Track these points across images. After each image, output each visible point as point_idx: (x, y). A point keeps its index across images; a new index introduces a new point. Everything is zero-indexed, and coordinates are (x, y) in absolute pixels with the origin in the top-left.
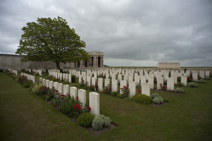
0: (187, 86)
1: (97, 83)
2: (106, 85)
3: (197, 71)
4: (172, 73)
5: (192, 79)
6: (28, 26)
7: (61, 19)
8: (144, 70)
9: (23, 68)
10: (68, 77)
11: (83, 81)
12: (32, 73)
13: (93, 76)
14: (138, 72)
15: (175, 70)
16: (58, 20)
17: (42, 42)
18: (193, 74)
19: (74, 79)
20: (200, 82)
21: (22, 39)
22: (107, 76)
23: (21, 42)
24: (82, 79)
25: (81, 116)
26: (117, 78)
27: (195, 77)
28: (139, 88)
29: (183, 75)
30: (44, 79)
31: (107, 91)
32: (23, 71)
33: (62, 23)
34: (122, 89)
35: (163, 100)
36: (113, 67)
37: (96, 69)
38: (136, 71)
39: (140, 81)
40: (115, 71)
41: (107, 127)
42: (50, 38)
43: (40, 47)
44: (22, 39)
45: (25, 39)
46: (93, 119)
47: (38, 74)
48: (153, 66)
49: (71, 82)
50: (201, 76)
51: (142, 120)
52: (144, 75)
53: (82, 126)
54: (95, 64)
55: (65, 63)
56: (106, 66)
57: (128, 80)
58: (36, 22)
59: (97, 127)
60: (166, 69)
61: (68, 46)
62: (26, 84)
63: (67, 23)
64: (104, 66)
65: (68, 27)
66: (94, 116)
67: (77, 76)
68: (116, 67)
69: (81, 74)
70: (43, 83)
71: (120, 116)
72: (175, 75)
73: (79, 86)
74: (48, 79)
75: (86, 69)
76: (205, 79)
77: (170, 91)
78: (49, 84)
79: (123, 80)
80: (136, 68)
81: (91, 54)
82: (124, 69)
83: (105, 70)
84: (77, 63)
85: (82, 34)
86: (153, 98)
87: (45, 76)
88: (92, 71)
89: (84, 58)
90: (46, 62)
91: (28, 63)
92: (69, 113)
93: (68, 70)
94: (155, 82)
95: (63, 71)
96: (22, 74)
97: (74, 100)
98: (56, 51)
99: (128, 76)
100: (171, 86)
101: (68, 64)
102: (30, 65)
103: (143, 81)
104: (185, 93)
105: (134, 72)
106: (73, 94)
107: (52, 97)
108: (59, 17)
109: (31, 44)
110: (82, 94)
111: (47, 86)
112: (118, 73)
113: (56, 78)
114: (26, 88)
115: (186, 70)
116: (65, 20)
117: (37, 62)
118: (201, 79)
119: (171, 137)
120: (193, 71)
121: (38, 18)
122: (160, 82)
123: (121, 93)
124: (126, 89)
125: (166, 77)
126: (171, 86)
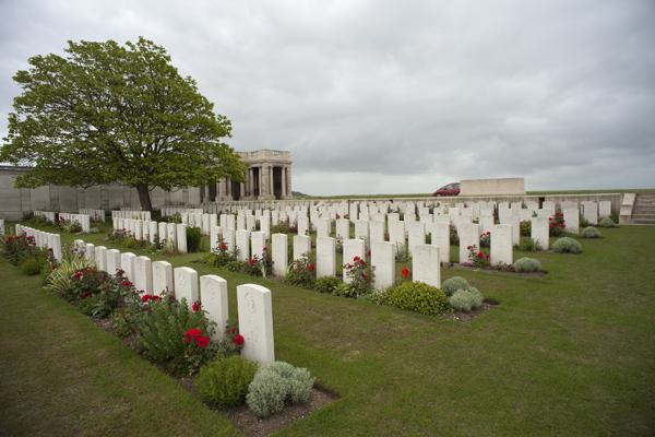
0: (550, 249)
1: (267, 250)
2: (297, 257)
3: (576, 204)
4: (503, 208)
5: (564, 226)
6: (34, 67)
7: (151, 47)
8: (418, 203)
9: (27, 209)
10: (175, 234)
11: (223, 247)
12: (57, 226)
13: (258, 228)
14: (398, 211)
15: (511, 200)
16: (138, 50)
17: (89, 122)
18: (565, 212)
19: (195, 239)
20: (585, 237)
21: (16, 112)
22: (303, 227)
23: (14, 123)
24: (220, 239)
25: (211, 370)
26: (333, 234)
27: (571, 221)
28: (403, 261)
29: (535, 215)
30: (91, 245)
31: (304, 275)
32: (29, 219)
33: (152, 59)
34: (350, 267)
35: (482, 298)
36: (320, 198)
37: (268, 205)
38: (394, 206)
39: (407, 240)
40: (327, 209)
41: (301, 403)
42: (113, 109)
43: (84, 139)
44: (16, 112)
45: (27, 111)
46: (252, 377)
47: (77, 229)
48: (417, 193)
49: (186, 250)
50: (586, 217)
51: (417, 371)
52: (418, 219)
53: (212, 404)
54: (264, 188)
55: (169, 190)
56: (298, 195)
57: (369, 237)
58: (65, 56)
59: (266, 409)
60: (484, 199)
61: (174, 135)
62: (31, 262)
63: (168, 58)
64: (294, 193)
65: (173, 72)
66: (253, 368)
67: (205, 229)
68: (330, 198)
69: (219, 224)
70: (88, 256)
71: (344, 359)
72: (512, 217)
73: (211, 261)
74: (91, 242)
75: (238, 205)
76: (597, 226)
77: (499, 268)
78: (107, 260)
79: (352, 237)
80: (391, 198)
81: (251, 159)
82: (355, 203)
83: (297, 208)
84: (207, 188)
85: (221, 101)
86: (449, 294)
87: (102, 232)
88: (254, 213)
89: (229, 172)
90: (104, 187)
91: (44, 192)
92: (171, 358)
93: (179, 210)
94: (454, 242)
95: (163, 214)
96: (20, 229)
97: (187, 313)
98: (136, 150)
99: (370, 220)
100: (502, 252)
101: (177, 194)
102: (51, 200)
103: (416, 241)
104: (546, 272)
105: (385, 211)
106: (184, 293)
107: (114, 304)
108: (142, 41)
109: (49, 128)
110: (210, 294)
111: (101, 268)
112: (338, 217)
113: (138, 238)
114: (30, 275)
115: (542, 200)
116: (162, 50)
117: (73, 189)
118: (589, 228)
119: (515, 428)
120: (562, 203)
121: (70, 42)
122: (469, 239)
123: (348, 280)
124: (364, 267)
125: (487, 224)
126: (502, 252)
